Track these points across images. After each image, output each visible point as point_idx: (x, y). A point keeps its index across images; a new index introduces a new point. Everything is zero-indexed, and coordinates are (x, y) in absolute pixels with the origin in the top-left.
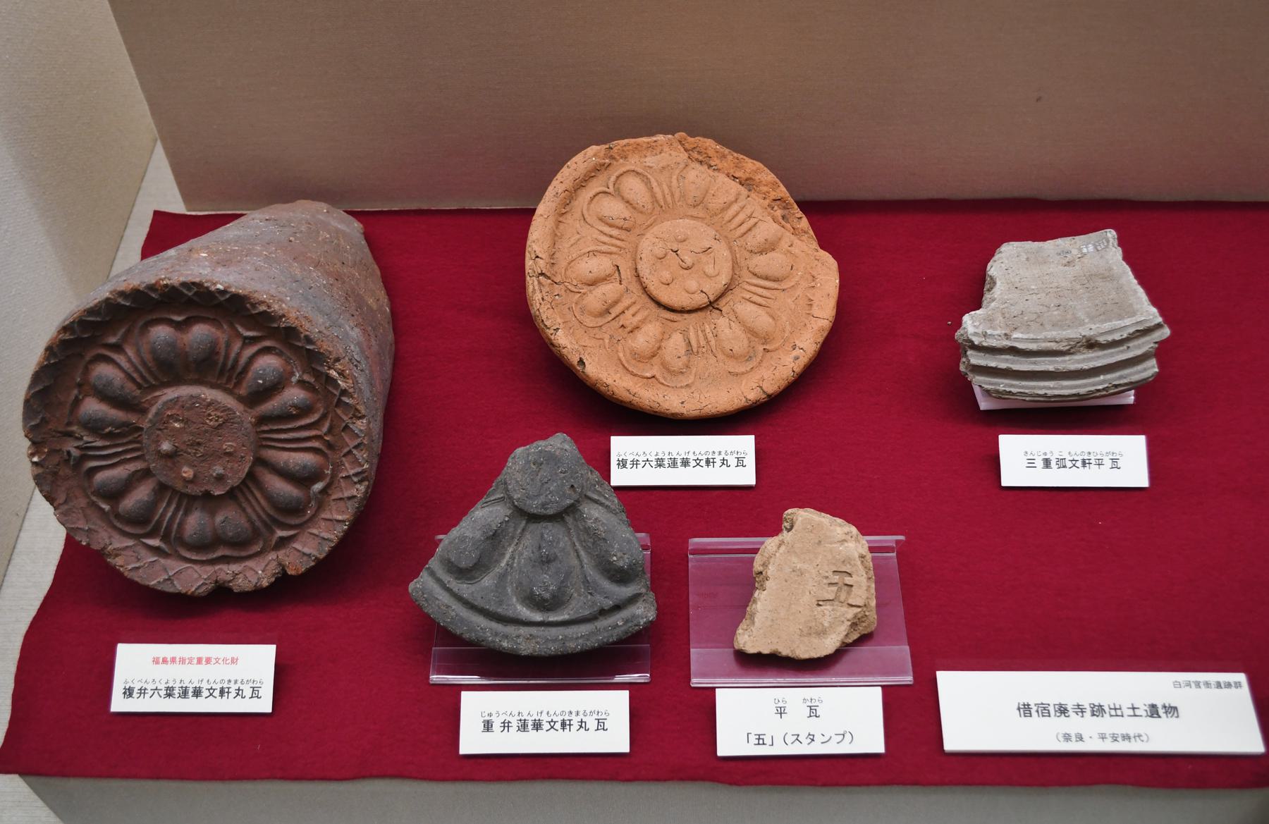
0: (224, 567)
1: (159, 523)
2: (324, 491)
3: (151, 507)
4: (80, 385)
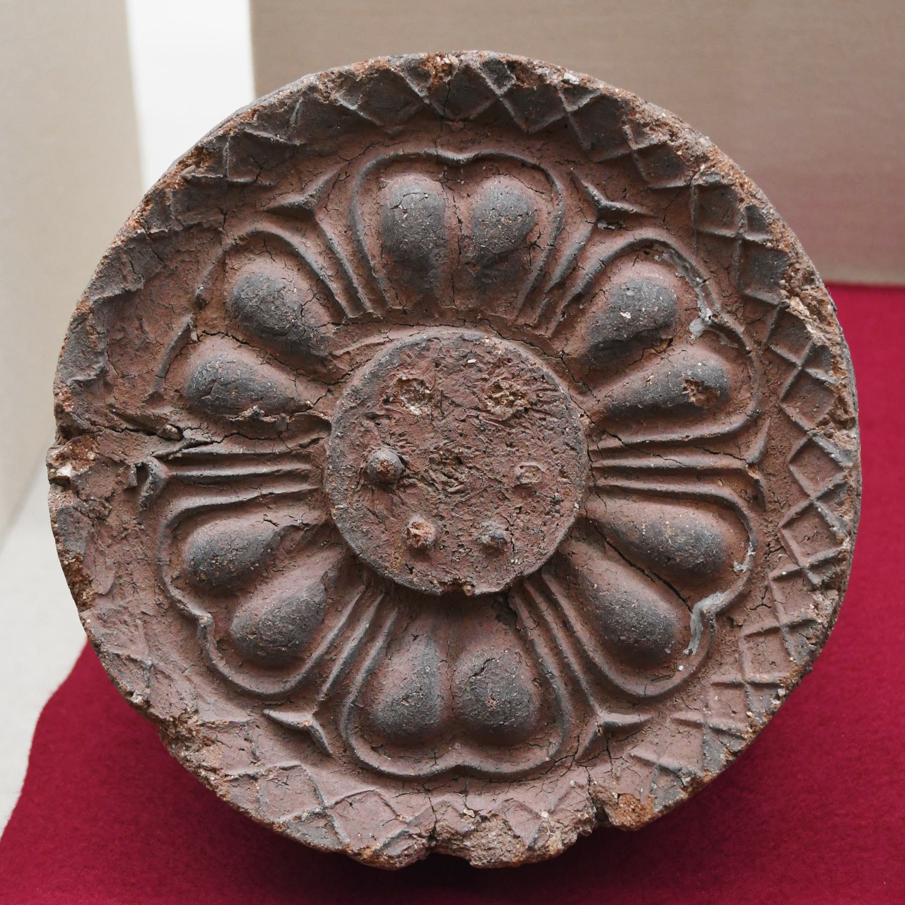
0: (455, 800)
1: (322, 665)
2: (725, 615)
3: (311, 621)
4: (200, 304)
